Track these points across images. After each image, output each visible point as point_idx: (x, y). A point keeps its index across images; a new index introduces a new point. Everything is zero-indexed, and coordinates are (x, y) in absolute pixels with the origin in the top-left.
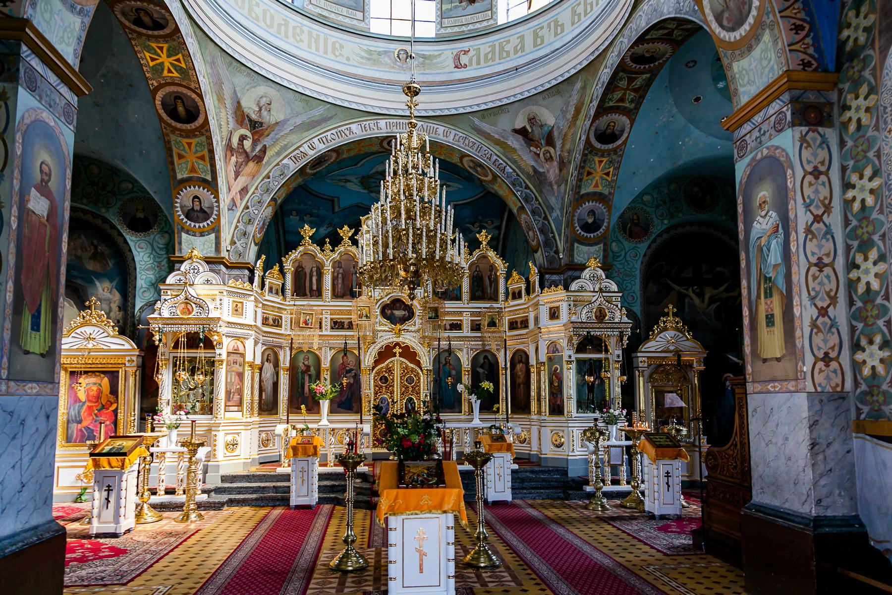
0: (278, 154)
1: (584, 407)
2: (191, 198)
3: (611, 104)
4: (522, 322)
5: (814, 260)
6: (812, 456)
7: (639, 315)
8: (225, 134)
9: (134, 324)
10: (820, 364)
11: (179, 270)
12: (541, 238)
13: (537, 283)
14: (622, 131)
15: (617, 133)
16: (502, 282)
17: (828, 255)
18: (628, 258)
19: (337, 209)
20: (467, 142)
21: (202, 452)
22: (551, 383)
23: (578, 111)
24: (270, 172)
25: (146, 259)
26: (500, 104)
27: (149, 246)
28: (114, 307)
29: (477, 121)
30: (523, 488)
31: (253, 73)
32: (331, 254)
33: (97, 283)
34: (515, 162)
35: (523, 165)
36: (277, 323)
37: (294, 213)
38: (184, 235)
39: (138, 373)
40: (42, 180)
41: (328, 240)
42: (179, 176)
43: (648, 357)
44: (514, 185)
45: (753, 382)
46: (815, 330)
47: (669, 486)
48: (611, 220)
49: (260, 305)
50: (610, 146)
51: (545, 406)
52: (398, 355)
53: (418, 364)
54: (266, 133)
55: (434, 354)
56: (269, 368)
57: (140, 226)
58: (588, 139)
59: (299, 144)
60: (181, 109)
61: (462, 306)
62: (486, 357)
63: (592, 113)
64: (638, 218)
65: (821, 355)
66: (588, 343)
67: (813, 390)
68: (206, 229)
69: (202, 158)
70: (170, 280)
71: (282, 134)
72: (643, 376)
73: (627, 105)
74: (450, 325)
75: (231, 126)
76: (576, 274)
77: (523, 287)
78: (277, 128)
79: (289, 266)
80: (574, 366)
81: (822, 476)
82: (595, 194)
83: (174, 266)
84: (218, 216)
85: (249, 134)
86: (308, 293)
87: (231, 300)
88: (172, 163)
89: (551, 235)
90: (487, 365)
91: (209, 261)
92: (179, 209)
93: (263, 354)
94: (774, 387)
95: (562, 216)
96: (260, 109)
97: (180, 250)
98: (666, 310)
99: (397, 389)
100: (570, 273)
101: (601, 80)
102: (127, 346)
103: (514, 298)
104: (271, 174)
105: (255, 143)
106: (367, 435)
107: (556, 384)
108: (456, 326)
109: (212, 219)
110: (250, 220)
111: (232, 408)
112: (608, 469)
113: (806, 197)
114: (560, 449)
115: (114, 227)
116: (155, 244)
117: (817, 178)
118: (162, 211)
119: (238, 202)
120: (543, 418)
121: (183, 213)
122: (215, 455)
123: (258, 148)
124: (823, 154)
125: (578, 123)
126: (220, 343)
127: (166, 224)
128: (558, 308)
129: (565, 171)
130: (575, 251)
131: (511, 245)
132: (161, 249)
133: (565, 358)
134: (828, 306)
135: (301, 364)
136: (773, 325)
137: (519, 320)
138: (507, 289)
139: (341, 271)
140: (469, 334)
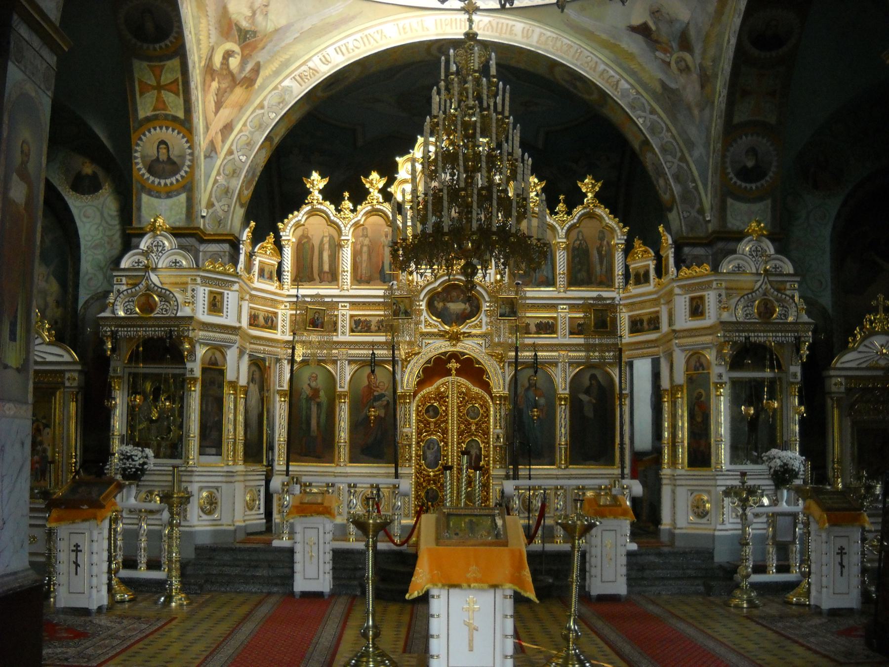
4: (650, 321)
8: (204, 52)
11: (137, 247)
13: (671, 261)
16: (619, 257)
20: (559, 44)
27: (98, 214)
28: (51, 300)
30: (643, 578)
32: (351, 215)
36: (270, 323)
38: (145, 198)
39: (79, 397)
40: (22, 163)
42: (142, 115)
43: (846, 377)
44: (633, 108)
47: (842, 566)
51: (682, 453)
52: (454, 372)
53: (486, 386)
54: (261, 45)
55: (509, 372)
59: (306, 58)
61: (555, 294)
62: (593, 377)
66: (746, 354)
68: (174, 188)
71: (283, 44)
75: (213, 40)
76: (731, 246)
77: (652, 265)
85: (236, 48)
89: (692, 185)
91: (176, 233)
92: (139, 160)
96: (254, 13)
97: (139, 217)
98: (874, 303)
99: (453, 426)
100: (720, 245)
102: (67, 358)
104: (266, 103)
106: (406, 495)
107: (699, 420)
108: (547, 328)
109: (183, 173)
110: (234, 172)
111: (208, 450)
112: (771, 550)
114: (704, 520)
119: (219, 144)
121: (143, 162)
123: (249, 67)
126: (192, 352)
128: (701, 298)
130: (728, 213)
131: (636, 199)
133: (714, 379)
137: (645, 318)
138: (627, 267)
139: (367, 242)
140: (567, 341)
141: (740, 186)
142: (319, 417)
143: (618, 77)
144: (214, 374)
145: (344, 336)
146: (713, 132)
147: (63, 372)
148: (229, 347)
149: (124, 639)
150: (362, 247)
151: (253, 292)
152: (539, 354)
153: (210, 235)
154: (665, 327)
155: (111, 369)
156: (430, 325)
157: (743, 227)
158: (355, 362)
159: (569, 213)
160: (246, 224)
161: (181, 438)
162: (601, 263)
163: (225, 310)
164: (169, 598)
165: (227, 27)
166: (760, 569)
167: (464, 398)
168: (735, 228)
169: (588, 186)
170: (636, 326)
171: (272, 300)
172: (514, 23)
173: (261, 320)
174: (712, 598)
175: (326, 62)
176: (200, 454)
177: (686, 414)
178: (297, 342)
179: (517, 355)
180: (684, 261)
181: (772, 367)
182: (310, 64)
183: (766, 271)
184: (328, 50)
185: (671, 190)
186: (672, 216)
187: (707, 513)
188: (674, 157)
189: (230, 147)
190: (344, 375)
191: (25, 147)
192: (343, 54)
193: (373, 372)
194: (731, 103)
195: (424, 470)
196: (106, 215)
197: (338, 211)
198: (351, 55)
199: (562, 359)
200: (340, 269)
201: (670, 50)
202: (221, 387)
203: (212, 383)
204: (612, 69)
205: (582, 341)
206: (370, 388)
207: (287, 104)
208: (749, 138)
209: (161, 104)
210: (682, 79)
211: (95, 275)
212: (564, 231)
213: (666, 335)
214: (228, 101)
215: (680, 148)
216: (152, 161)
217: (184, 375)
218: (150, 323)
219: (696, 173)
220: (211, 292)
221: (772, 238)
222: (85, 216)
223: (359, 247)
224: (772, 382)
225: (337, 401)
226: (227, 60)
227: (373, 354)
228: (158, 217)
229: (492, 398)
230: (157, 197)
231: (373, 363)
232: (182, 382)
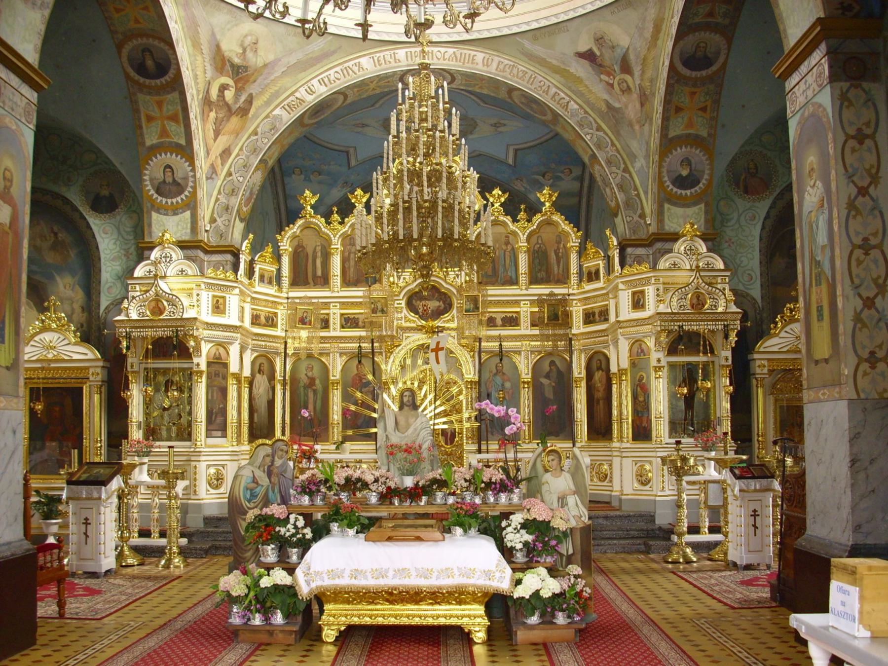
0: (268, 103)
1: (679, 429)
3: (697, 20)
4: (601, 313)
5: (858, 241)
6: (852, 474)
8: (202, 86)
9: (99, 328)
10: (865, 366)
11: (148, 258)
13: (617, 260)
14: (718, 53)
15: (710, 55)
16: (574, 258)
17: (875, 234)
18: (743, 223)
19: (353, 163)
20: (515, 71)
21: (181, 485)
22: (635, 398)
23: (657, 29)
24: (258, 126)
25: (111, 246)
26: (556, 21)
27: (116, 231)
28: (77, 307)
29: (527, 44)
31: (234, 9)
32: (339, 227)
33: (58, 279)
36: (271, 322)
37: (297, 171)
38: (154, 215)
39: (103, 389)
40: (5, 187)
41: (335, 209)
42: (148, 143)
43: (769, 360)
44: (581, 126)
45: (809, 388)
46: (859, 325)
49: (249, 299)
50: (704, 73)
51: (628, 430)
54: (251, 80)
56: (261, 381)
57: (104, 205)
59: (294, 89)
60: (149, 63)
61: (518, 292)
62: (552, 363)
64: (756, 167)
65: (866, 355)
66: (682, 341)
67: (855, 397)
70: (139, 272)
71: (272, 78)
72: (763, 386)
73: (719, 20)
74: (503, 319)
75: (209, 74)
76: (667, 246)
77: (601, 264)
78: (266, 71)
79: (286, 245)
80: (664, 373)
81: (863, 497)
83: (142, 254)
84: (194, 188)
85: (230, 82)
87: (211, 294)
88: (141, 127)
90: (554, 374)
91: (183, 245)
92: (148, 183)
93: (253, 363)
96: (245, 50)
97: (150, 233)
100: (659, 245)
102: (90, 356)
104: (259, 130)
105: (239, 91)
107: (641, 399)
108: (512, 321)
109: (186, 193)
110: (233, 191)
111: (214, 433)
112: (705, 513)
113: (848, 166)
114: (647, 488)
115: (76, 209)
117: (861, 143)
120: (624, 445)
121: (153, 188)
122: (195, 491)
123: (243, 98)
124: (868, 114)
126: (198, 349)
129: (647, 106)
131: (584, 206)
132: (128, 233)
133: (654, 363)
134: (876, 296)
136: (822, 319)
137: (597, 311)
138: (580, 267)
140: (528, 332)
142: (315, 402)
144: (218, 366)
145: (335, 331)
147: (87, 368)
148: (231, 344)
149: (131, 595)
150: (349, 254)
151: (254, 295)
152: (503, 344)
153: (212, 247)
154: (612, 318)
157: (679, 229)
158: (345, 354)
159: (529, 221)
160: (244, 237)
161: (190, 424)
163: (227, 311)
164: (169, 561)
165: (221, 63)
166: (694, 529)
168: (672, 230)
169: (546, 196)
170: (589, 318)
171: (275, 302)
172: (475, 53)
173: (263, 319)
174: (652, 556)
176: (207, 437)
177: (630, 395)
178: (289, 338)
179: (501, 345)
181: (705, 353)
182: (297, 95)
183: (698, 267)
185: (616, 197)
186: (618, 220)
187: (649, 481)
189: (229, 170)
190: (336, 366)
191: (8, 174)
192: (326, 85)
193: (360, 362)
194: (665, 119)
195: (442, 446)
196: (123, 232)
199: (525, 351)
202: (225, 378)
203: (217, 375)
205: (537, 332)
208: (684, 149)
209: (164, 133)
210: (624, 99)
213: (613, 325)
214: (226, 129)
215: (623, 159)
216: (160, 183)
217: (192, 368)
218: (160, 324)
220: (214, 296)
221: (705, 238)
223: (347, 254)
224: (706, 365)
225: (330, 388)
226: (223, 93)
227: (360, 346)
228: (165, 231)
230: (165, 215)
232: (190, 374)
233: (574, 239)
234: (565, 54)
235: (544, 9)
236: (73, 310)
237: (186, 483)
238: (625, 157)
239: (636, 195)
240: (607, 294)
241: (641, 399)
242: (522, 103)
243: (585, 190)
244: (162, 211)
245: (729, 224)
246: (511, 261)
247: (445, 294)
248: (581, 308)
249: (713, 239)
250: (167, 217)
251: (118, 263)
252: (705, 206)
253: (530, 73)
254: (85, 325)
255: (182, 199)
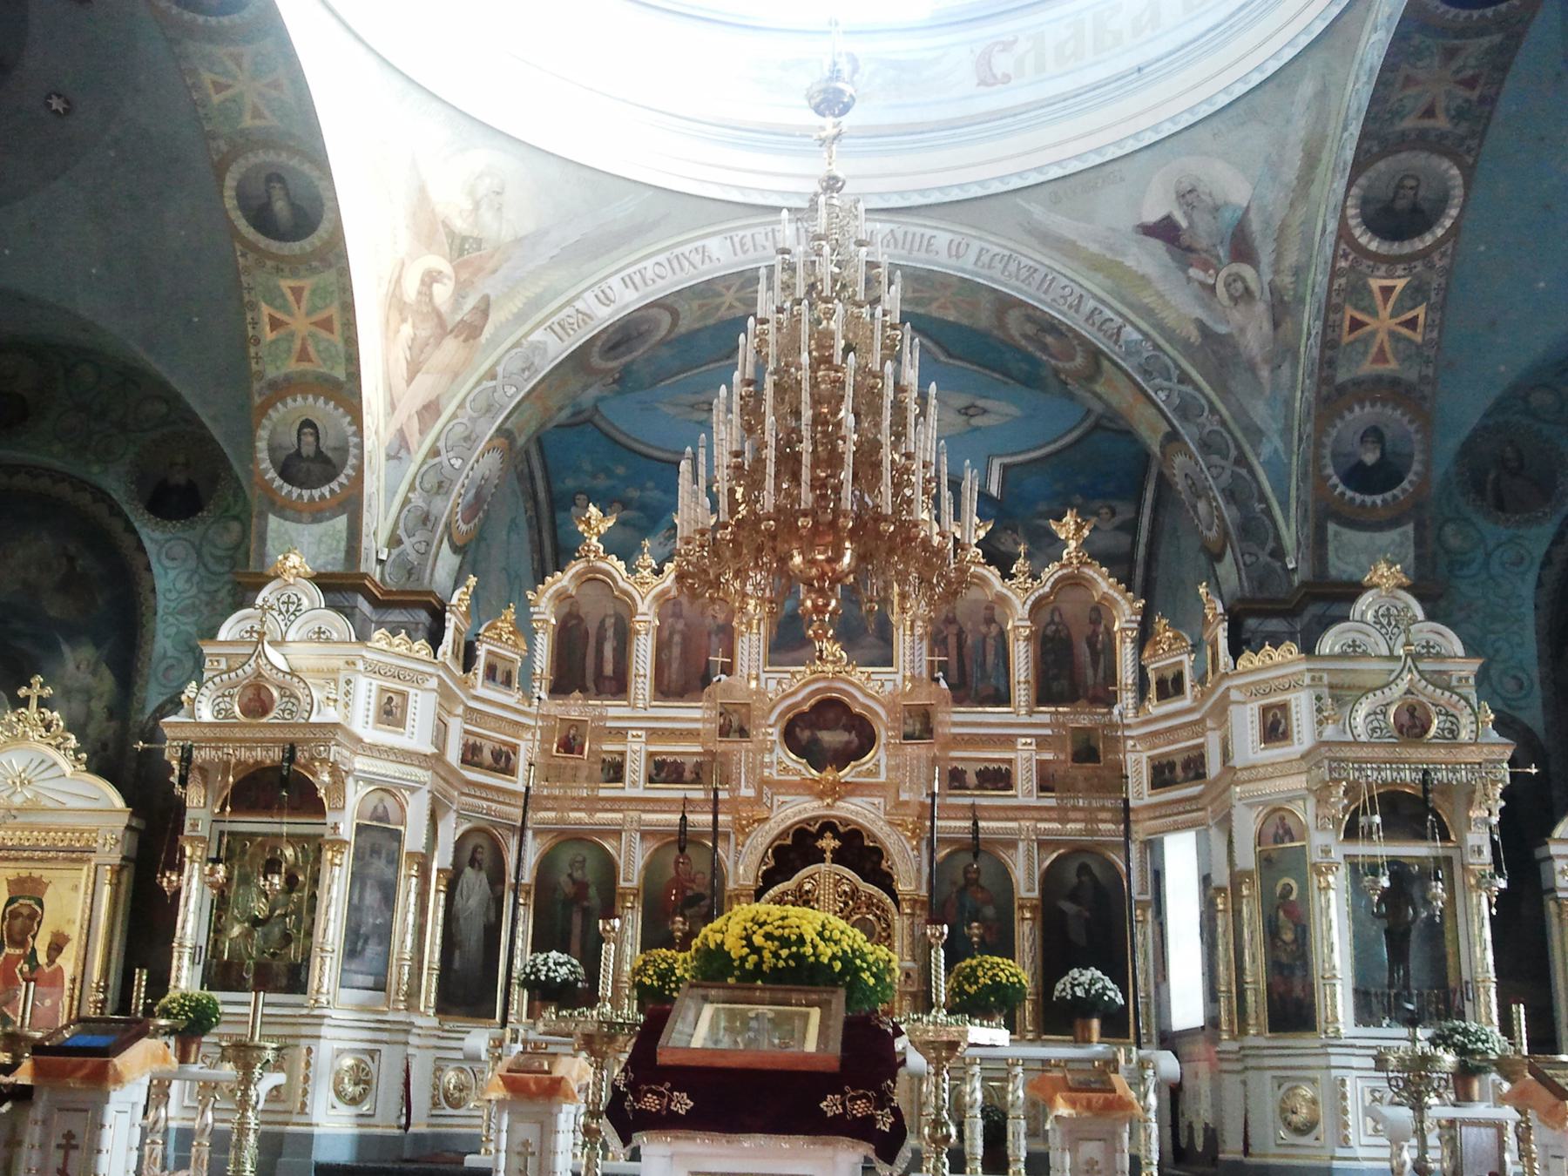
0: (520, 317)
2: (297, 426)
4: (1187, 765)
7: (1541, 734)
12: (1230, 514)
13: (1223, 644)
14: (1443, 202)
15: (1426, 206)
18: (1495, 568)
20: (1013, 267)
22: (1272, 932)
24: (497, 363)
27: (192, 551)
28: (98, 707)
32: (654, 580)
33: (65, 649)
34: (1147, 312)
35: (1170, 319)
36: (503, 762)
38: (273, 521)
39: (125, 876)
44: (1147, 373)
48: (1431, 462)
49: (460, 710)
52: (828, 855)
53: (885, 881)
56: (475, 882)
58: (1344, 233)
59: (572, 293)
60: (280, 206)
61: (1012, 719)
63: (1349, 155)
69: (326, 324)
74: (979, 774)
76: (1336, 610)
82: (1378, 380)
84: (359, 470)
85: (445, 266)
86: (590, 684)
89: (1259, 507)
93: (459, 845)
94: (1443, 255)
95: (1289, 452)
100: (1314, 609)
101: (1367, 66)
103: (1163, 695)
104: (500, 369)
107: (1288, 936)
108: (998, 779)
109: (342, 479)
110: (440, 485)
115: (115, 510)
116: (206, 550)
118: (230, 468)
123: (471, 302)
125: (1315, 190)
127: (235, 496)
129: (1287, 325)
130: (1331, 548)
135: (563, 879)
137: (1179, 760)
138: (1142, 671)
139: (680, 626)
141: (1352, 500)
143: (1120, 321)
144: (379, 838)
145: (635, 784)
146: (1297, 404)
150: (671, 635)
153: (390, 593)
154: (1213, 767)
155: (187, 823)
156: (786, 770)
162: (1095, 663)
167: (846, 904)
170: (1162, 775)
171: (517, 723)
173: (487, 756)
175: (605, 300)
176: (342, 986)
180: (1248, 643)
182: (579, 305)
184: (611, 281)
185: (1221, 518)
188: (1225, 457)
192: (636, 288)
197: (631, 570)
198: (649, 289)
200: (634, 671)
201: (1215, 261)
202: (394, 861)
203: (375, 851)
204: (1111, 308)
205: (1052, 802)
206: (680, 883)
207: (537, 371)
210: (1237, 315)
211: (180, 661)
212: (1027, 607)
216: (289, 457)
219: (1266, 485)
220: (383, 690)
222: (168, 557)
223: (666, 634)
226: (430, 287)
229: (897, 903)
231: (683, 838)
232: (314, 848)
233: (1125, 614)
234: (1113, 230)
235: (1075, 139)
236: (89, 715)
237: (279, 1078)
238: (1239, 435)
239: (1262, 511)
240: (1202, 721)
241: (1288, 936)
242: (1025, 336)
243: (1141, 551)
244: (289, 513)
245: (1466, 572)
246: (996, 655)
247: (861, 717)
248: (1144, 757)
249: (1434, 590)
250: (300, 526)
251: (192, 619)
252: (1416, 529)
253: (1043, 270)
254: (111, 745)
255: (332, 491)
